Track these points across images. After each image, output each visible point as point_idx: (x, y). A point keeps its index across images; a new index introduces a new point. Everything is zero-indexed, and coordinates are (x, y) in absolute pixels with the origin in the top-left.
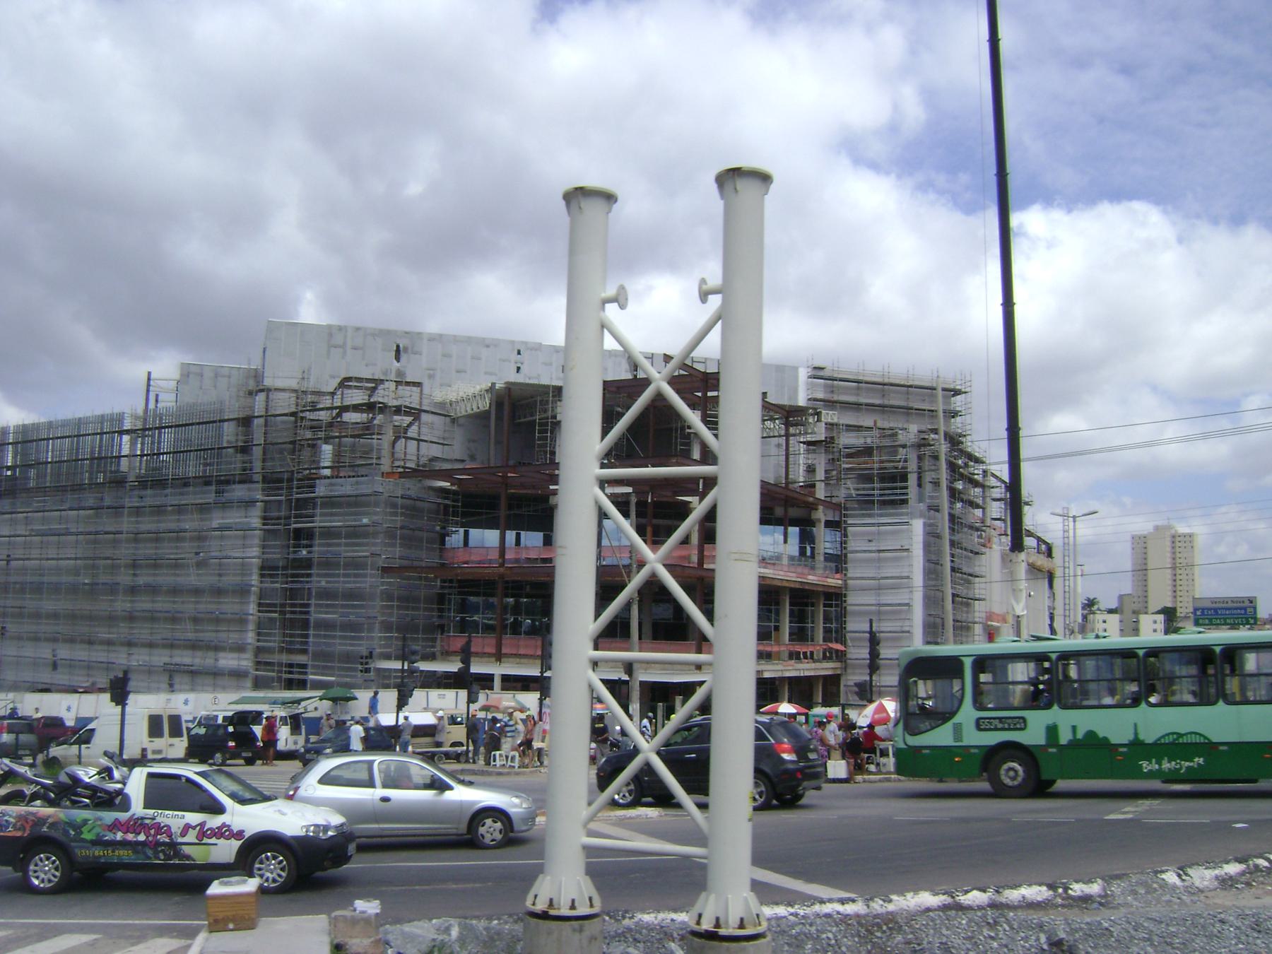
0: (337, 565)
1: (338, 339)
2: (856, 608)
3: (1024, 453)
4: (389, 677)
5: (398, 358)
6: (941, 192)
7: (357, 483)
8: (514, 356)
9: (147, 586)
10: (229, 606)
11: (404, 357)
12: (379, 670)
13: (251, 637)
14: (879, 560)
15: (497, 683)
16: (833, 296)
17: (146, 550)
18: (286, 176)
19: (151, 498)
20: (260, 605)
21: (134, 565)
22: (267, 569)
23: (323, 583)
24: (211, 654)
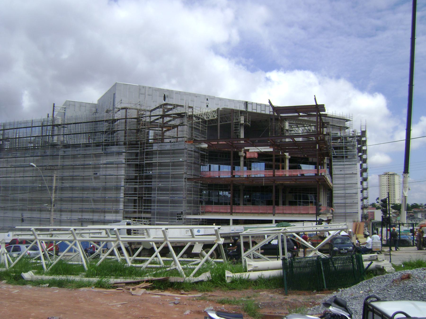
0: (168, 178)
1: (143, 91)
2: (336, 195)
3: (412, 137)
6: (244, 65)
7: (174, 145)
12: (185, 219)
13: (121, 206)
15: (231, 222)
22: (128, 180)
23: (160, 185)
24: (103, 214)
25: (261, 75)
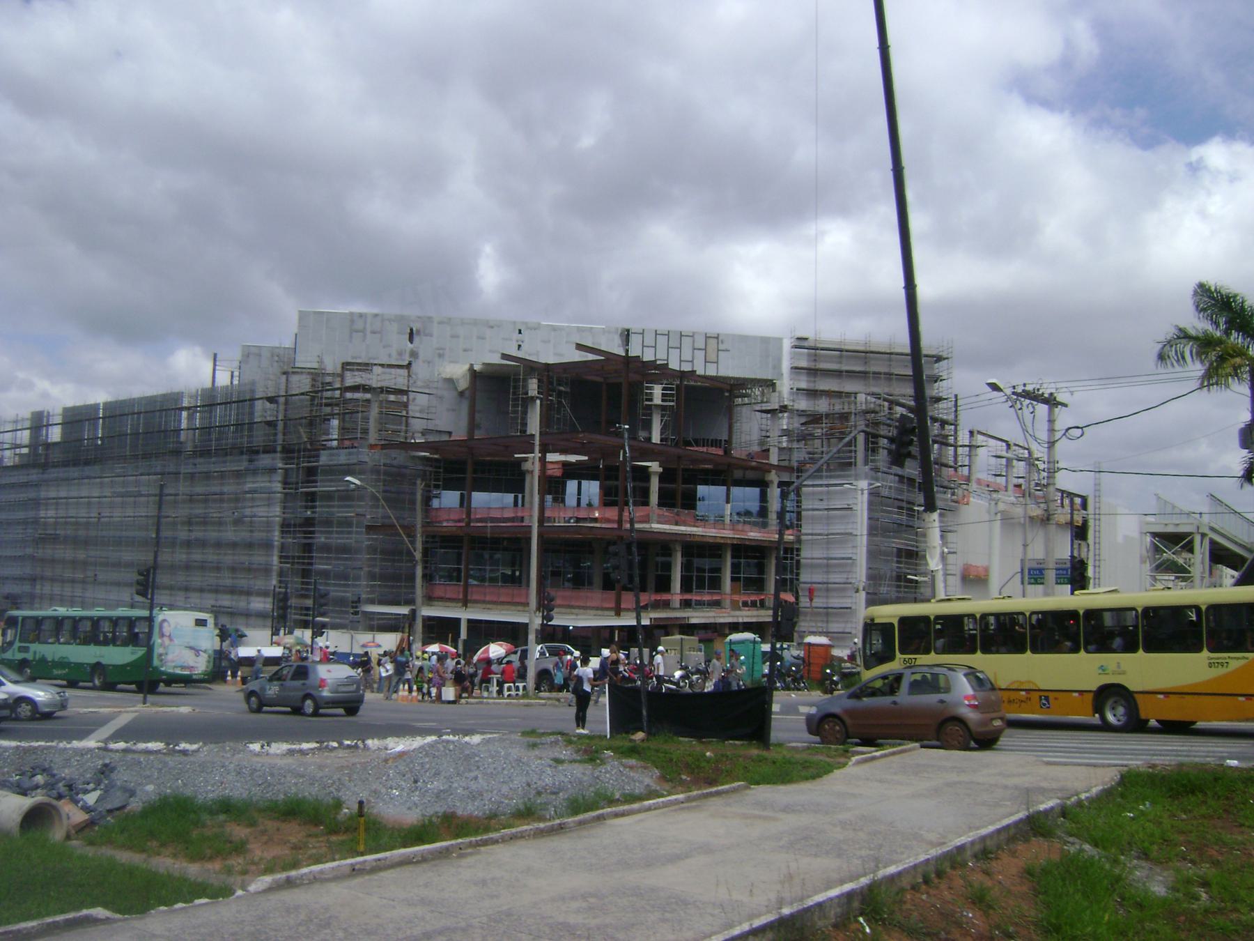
4: (372, 619)
5: (411, 339)
8: (516, 335)
9: (197, 540)
10: (258, 558)
11: (416, 339)
14: (828, 518)
16: (1006, 236)
17: (199, 510)
18: (463, 136)
19: (203, 465)
20: (281, 557)
21: (190, 523)
22: (286, 527)
24: (243, 598)
25: (1172, 157)
